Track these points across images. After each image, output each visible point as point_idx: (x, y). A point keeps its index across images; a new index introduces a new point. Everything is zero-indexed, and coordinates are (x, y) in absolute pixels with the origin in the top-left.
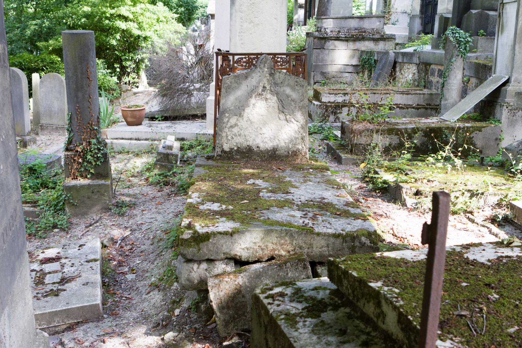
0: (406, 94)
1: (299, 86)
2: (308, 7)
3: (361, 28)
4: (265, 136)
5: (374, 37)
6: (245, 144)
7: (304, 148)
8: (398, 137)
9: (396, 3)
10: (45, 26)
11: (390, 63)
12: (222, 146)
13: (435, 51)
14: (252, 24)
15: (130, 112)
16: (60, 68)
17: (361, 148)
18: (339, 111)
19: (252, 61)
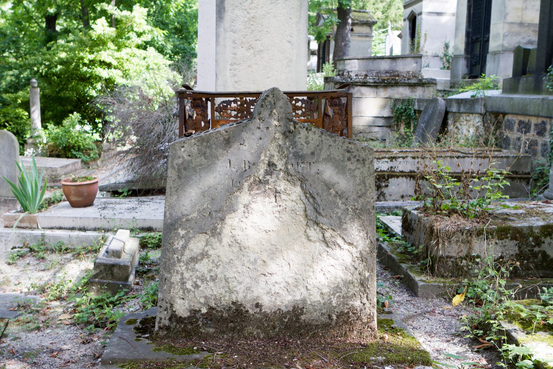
0: (481, 157)
1: (353, 160)
2: (321, 53)
3: (394, 71)
4: (274, 278)
5: (410, 81)
6: (226, 300)
7: (368, 305)
8: (515, 242)
9: (425, 46)
10: (24, 77)
11: (440, 113)
12: (172, 305)
13: (511, 96)
14: (252, 51)
15: (74, 188)
16: (26, 124)
17: (450, 263)
18: (383, 184)
19: (247, 106)
